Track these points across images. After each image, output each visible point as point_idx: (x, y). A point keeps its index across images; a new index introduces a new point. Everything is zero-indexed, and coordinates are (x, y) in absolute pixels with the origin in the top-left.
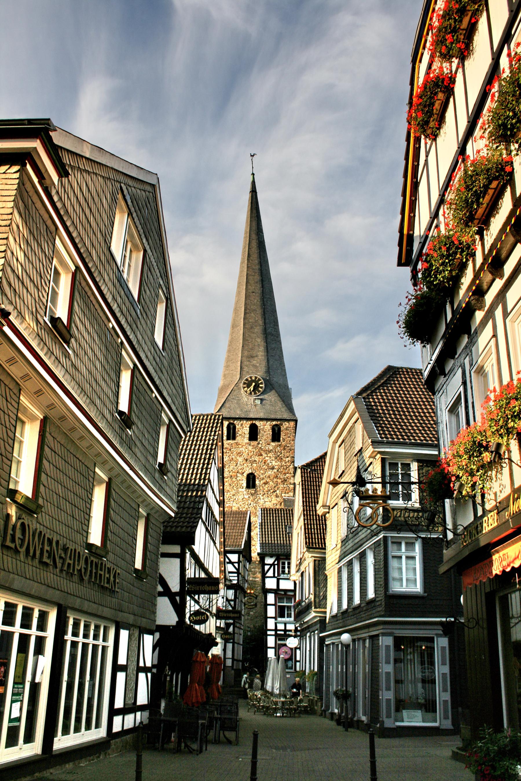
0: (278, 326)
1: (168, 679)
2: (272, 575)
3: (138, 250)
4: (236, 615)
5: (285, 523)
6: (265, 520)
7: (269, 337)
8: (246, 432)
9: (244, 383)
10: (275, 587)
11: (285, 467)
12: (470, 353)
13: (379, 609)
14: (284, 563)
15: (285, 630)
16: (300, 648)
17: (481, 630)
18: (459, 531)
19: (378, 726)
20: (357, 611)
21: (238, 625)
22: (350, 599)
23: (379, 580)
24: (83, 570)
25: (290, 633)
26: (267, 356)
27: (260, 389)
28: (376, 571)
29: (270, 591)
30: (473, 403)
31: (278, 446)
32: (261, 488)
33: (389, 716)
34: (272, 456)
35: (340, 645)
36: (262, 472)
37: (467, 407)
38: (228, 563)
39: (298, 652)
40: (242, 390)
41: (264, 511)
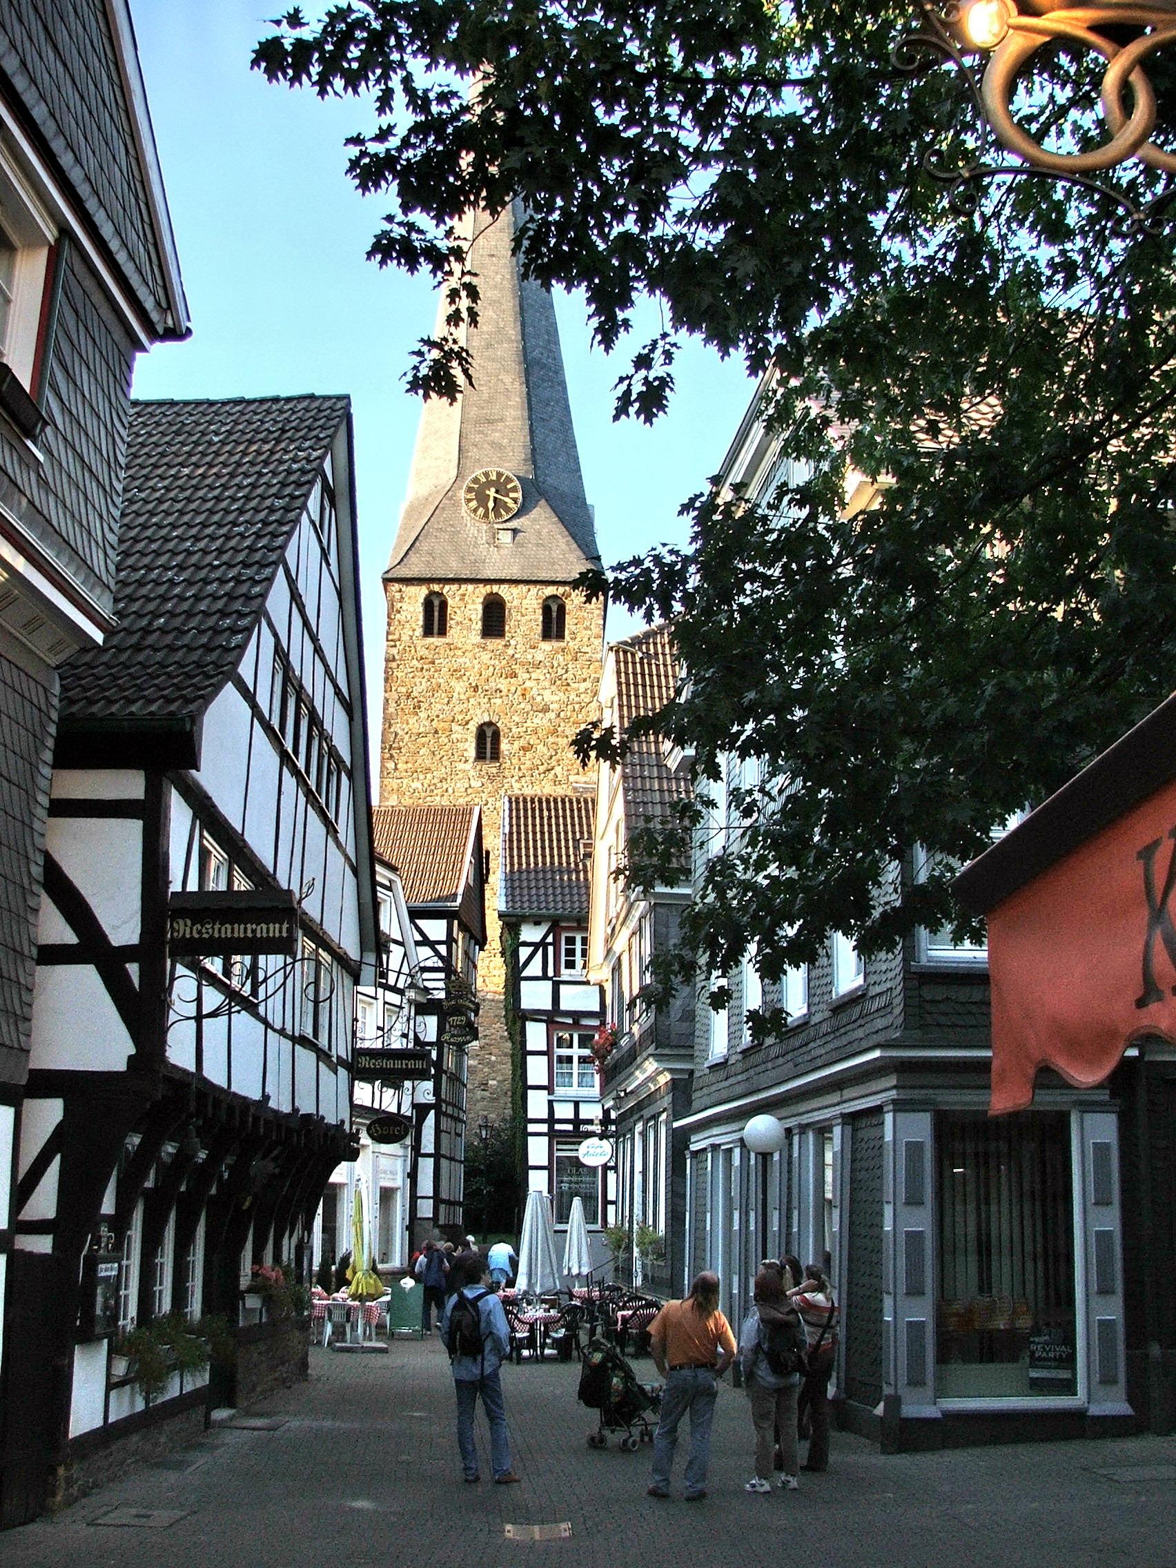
0: (557, 343)
2: (540, 974)
5: (574, 833)
6: (518, 826)
8: (473, 617)
9: (470, 490)
11: (577, 707)
13: (880, 1023)
14: (571, 941)
15: (577, 1121)
16: (615, 1168)
19: (880, 1410)
25: (590, 1128)
26: (530, 418)
29: (535, 1015)
31: (557, 652)
32: (515, 761)
33: (916, 1381)
34: (542, 678)
35: (737, 1152)
36: (516, 718)
38: (417, 943)
39: (611, 1176)
40: (464, 507)
41: (517, 803)
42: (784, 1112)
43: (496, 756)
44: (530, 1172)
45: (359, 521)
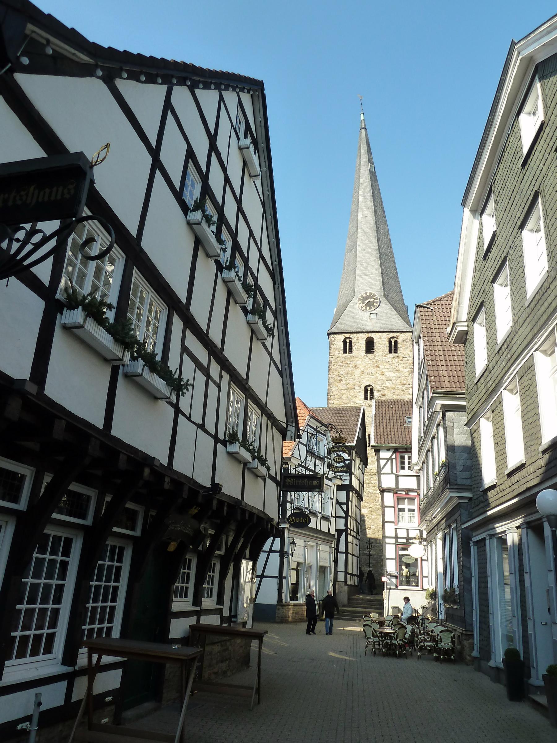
7: (384, 256)
9: (360, 300)
14: (403, 457)
27: (375, 304)
29: (388, 490)
39: (425, 563)
44: (387, 560)
45: (276, 195)
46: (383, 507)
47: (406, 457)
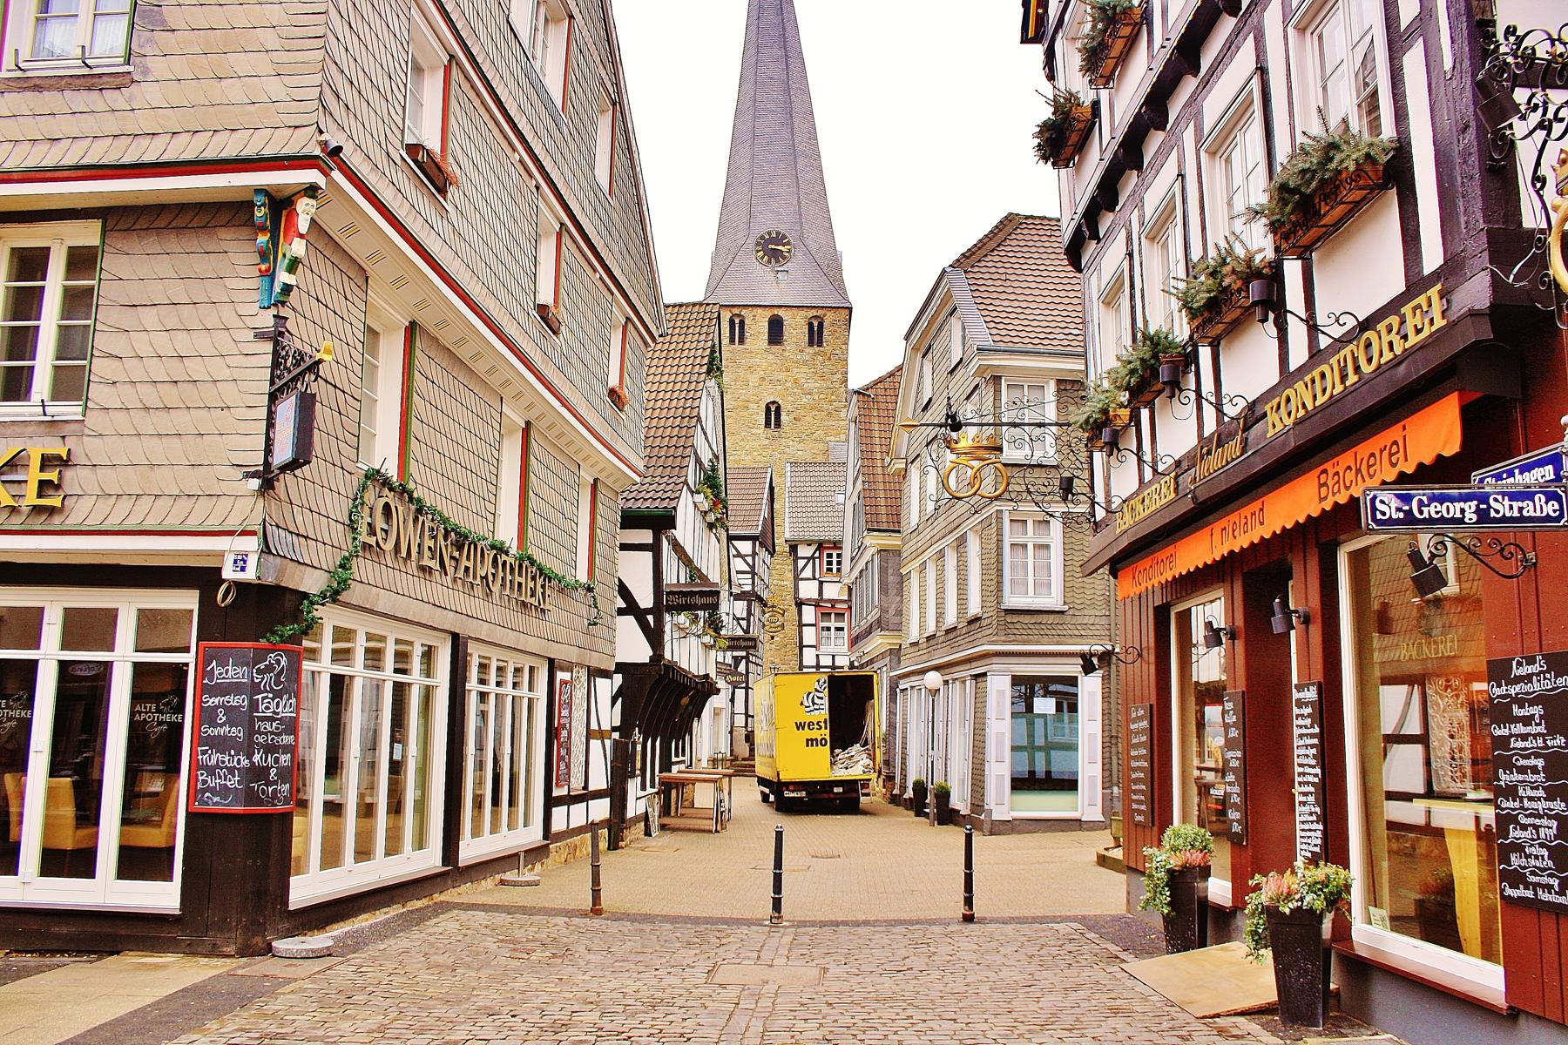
1: (639, 748)
3: (558, 21)
4: (750, 643)
10: (816, 596)
12: (1140, 204)
14: (830, 556)
17: (1145, 666)
18: (1114, 506)
20: (951, 636)
21: (754, 659)
22: (940, 616)
23: (988, 583)
24: (490, 578)
28: (984, 568)
30: (1142, 290)
35: (923, 690)
37: (1132, 297)
42: (943, 672)
43: (778, 424)
46: (801, 625)
47: (835, 555)
